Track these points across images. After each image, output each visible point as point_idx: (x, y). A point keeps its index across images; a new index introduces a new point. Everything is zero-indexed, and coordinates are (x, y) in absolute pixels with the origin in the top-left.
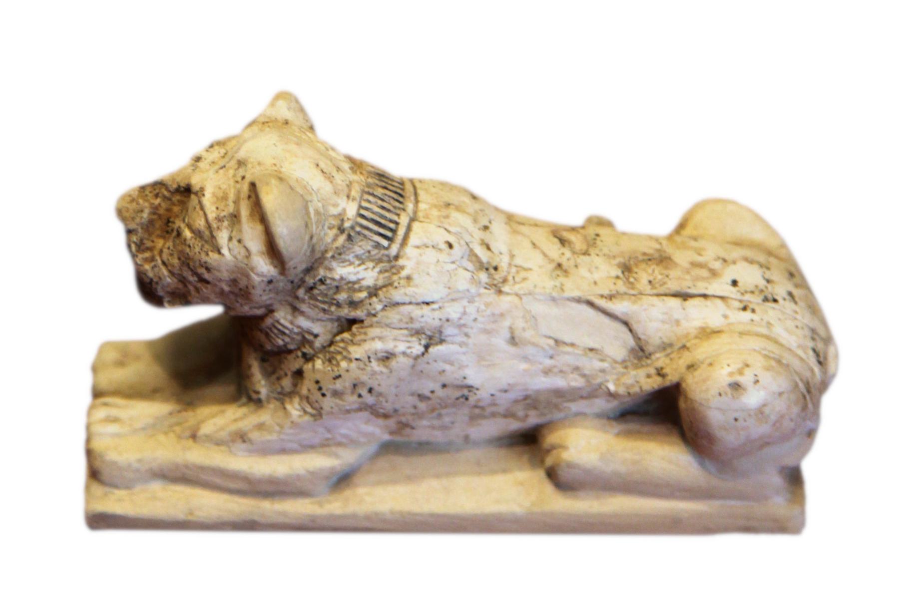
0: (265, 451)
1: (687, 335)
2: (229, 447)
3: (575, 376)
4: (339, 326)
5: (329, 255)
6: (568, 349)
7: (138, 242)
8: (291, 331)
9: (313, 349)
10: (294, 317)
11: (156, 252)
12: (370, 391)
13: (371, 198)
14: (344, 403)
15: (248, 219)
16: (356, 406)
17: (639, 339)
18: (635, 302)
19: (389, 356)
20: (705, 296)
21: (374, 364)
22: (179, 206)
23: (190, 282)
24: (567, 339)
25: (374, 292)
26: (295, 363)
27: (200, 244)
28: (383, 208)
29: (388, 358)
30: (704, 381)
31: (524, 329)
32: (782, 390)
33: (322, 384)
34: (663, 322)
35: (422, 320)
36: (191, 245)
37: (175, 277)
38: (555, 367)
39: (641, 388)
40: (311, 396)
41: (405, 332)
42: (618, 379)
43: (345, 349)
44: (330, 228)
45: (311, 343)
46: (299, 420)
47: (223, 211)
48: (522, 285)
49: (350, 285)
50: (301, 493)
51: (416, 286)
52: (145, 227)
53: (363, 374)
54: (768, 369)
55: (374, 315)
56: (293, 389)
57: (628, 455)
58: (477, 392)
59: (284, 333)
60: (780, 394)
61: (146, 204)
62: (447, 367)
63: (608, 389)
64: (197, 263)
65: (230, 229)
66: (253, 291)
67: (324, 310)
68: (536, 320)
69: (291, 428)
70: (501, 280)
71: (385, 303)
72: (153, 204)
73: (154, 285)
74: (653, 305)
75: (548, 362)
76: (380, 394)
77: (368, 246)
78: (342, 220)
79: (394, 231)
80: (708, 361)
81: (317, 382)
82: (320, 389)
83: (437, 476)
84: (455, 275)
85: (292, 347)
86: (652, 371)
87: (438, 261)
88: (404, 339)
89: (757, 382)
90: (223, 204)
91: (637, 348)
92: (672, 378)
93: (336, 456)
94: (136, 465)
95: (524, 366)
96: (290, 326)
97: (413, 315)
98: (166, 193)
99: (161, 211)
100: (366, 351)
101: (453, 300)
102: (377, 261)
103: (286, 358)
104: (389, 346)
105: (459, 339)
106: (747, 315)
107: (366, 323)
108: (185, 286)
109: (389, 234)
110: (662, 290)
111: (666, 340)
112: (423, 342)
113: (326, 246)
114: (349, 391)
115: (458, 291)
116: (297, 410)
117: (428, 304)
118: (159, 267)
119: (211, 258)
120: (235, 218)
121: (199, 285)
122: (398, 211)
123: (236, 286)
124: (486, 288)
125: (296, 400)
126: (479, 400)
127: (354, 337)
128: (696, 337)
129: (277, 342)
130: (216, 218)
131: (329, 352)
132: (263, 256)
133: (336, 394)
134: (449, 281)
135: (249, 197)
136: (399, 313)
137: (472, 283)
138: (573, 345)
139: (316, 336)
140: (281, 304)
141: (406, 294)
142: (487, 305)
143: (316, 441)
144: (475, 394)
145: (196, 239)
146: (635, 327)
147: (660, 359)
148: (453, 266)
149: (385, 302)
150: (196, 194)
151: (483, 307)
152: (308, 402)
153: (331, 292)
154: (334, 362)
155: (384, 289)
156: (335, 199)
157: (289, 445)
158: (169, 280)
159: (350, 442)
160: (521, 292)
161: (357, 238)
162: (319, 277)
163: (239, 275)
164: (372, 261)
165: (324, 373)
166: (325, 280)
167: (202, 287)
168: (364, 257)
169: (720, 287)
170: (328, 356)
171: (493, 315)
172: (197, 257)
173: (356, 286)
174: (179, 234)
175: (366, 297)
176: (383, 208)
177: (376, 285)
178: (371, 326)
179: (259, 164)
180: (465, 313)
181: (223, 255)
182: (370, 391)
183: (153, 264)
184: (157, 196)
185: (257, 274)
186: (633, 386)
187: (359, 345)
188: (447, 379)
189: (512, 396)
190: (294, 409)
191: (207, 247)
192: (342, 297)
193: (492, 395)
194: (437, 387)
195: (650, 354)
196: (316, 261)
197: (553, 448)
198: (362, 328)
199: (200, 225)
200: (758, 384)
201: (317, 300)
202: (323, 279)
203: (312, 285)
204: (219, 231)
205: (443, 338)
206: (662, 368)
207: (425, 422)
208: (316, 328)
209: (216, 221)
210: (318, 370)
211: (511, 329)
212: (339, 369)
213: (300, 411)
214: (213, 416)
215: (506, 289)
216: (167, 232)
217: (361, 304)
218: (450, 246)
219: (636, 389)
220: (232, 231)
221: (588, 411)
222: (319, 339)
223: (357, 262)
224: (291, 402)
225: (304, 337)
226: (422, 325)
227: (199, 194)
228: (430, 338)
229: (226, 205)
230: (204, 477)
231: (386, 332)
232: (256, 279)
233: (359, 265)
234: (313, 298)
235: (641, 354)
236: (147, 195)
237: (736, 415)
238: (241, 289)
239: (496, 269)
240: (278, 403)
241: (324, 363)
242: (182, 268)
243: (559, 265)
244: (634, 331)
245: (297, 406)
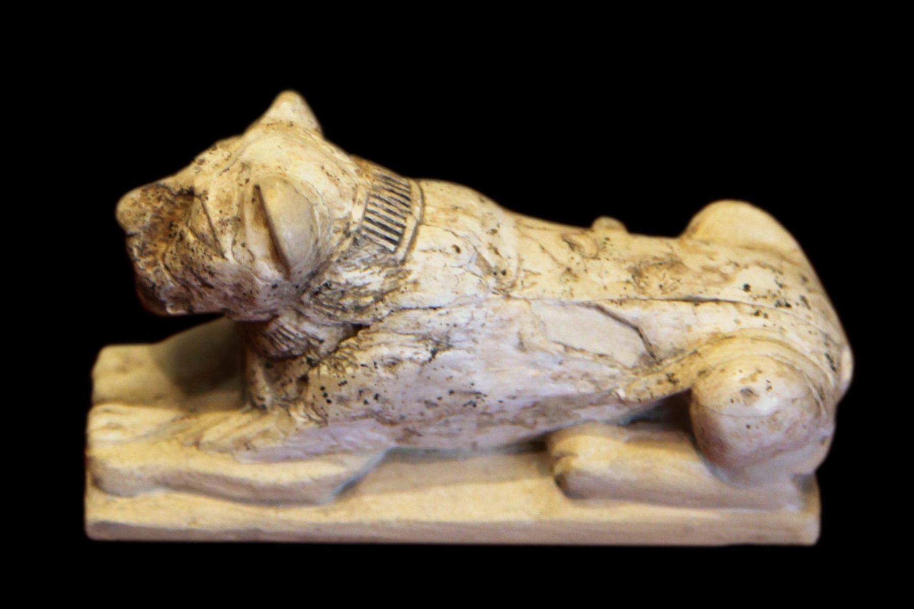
0: (269, 458)
1: (698, 341)
2: (233, 454)
3: (585, 382)
4: (344, 331)
5: (335, 259)
6: (578, 355)
7: (140, 246)
8: (296, 336)
9: (319, 355)
10: (299, 322)
11: (159, 257)
12: (377, 397)
13: (377, 201)
15: (252, 223)
16: (361, 413)
17: (650, 345)
18: (645, 307)
19: (396, 362)
20: (717, 301)
21: (380, 370)
22: (182, 209)
23: (193, 287)
24: (577, 345)
25: (380, 297)
26: (300, 369)
27: (203, 248)
28: (389, 211)
29: (394, 364)
30: (716, 387)
31: (533, 335)
32: (795, 397)
33: (327, 391)
34: (674, 327)
35: (430, 325)
36: (195, 249)
37: (178, 282)
38: (564, 373)
39: (651, 394)
40: (316, 403)
41: (412, 337)
42: (628, 386)
43: (351, 354)
44: (336, 232)
45: (316, 349)
46: (304, 427)
47: (227, 214)
48: (531, 290)
49: (356, 290)
50: (306, 501)
51: (423, 291)
52: (147, 231)
53: (369, 380)
54: (781, 375)
55: (381, 321)
56: (298, 396)
57: (638, 463)
58: (485, 399)
59: (289, 339)
60: (794, 401)
61: (149, 208)
62: (455, 373)
63: (619, 396)
64: (201, 268)
65: (234, 233)
66: (257, 296)
67: (330, 316)
68: (545, 325)
69: (296, 435)
70: (509, 285)
71: (392, 308)
72: (156, 207)
73: (157, 290)
74: (664, 311)
75: (557, 368)
76: (387, 401)
77: (374, 250)
78: (348, 224)
79: (400, 235)
80: (720, 367)
81: (323, 388)
82: (325, 395)
83: (445, 484)
84: (463, 279)
85: (296, 352)
86: (663, 377)
87: (445, 265)
88: (411, 344)
89: (769, 388)
90: (226, 207)
91: (648, 354)
92: (683, 384)
93: (342, 463)
94: (138, 473)
95: (532, 372)
96: (295, 332)
97: (420, 320)
98: (168, 196)
99: (164, 215)
100: (372, 357)
101: (461, 305)
102: (383, 265)
103: (291, 364)
104: (396, 351)
105: (467, 344)
106: (760, 320)
107: (372, 329)
108: (188, 291)
109: (396, 238)
110: (673, 295)
111: (677, 346)
112: (431, 348)
113: (331, 250)
114: (355, 398)
115: (466, 296)
116: (302, 416)
117: (435, 309)
118: (161, 271)
119: (214, 263)
120: (239, 221)
121: (202, 290)
122: (405, 215)
123: (240, 291)
124: (494, 293)
125: (301, 407)
126: (487, 407)
127: (360, 343)
128: (708, 343)
129: (282, 348)
130: (220, 222)
131: (335, 358)
132: (268, 261)
133: (342, 400)
134: (456, 286)
135: (253, 200)
136: (405, 318)
137: (480, 288)
138: (582, 351)
139: (321, 342)
140: (286, 309)
141: (412, 299)
142: (495, 310)
143: (322, 448)
144: (483, 400)
145: (199, 243)
146: (645, 332)
147: (671, 365)
148: (461, 271)
149: (392, 307)
150: (199, 197)
151: (491, 312)
152: (313, 409)
153: (336, 297)
155: (391, 294)
156: (341, 202)
157: (294, 453)
158: (171, 285)
159: (356, 450)
160: (530, 297)
161: (363, 242)
162: (325, 282)
163: (243, 280)
164: (379, 265)
165: (330, 379)
166: (331, 285)
167: (206, 292)
168: (370, 261)
169: (732, 292)
170: (333, 362)
171: (502, 320)
172: (200, 262)
173: (362, 291)
174: (182, 238)
175: (372, 302)
176: (389, 211)
177: (382, 290)
178: (377, 331)
179: (264, 166)
180: (472, 318)
181: (227, 259)
182: (377, 397)
183: (155, 268)
184: (159, 199)
185: (262, 279)
186: (643, 392)
187: (365, 350)
188: (455, 385)
189: (520, 402)
190: (299, 416)
191: (210, 251)
192: (348, 301)
193: (500, 402)
194: (444, 393)
195: (661, 360)
196: (321, 265)
197: (562, 455)
198: (368, 333)
199: (203, 229)
200: (771, 391)
201: (322, 305)
202: (329, 284)
203: (317, 289)
204: (223, 235)
205: (450, 343)
206: (673, 375)
207: (432, 430)
208: (322, 334)
209: (220, 225)
210: (324, 377)
211: (520, 335)
212: (345, 375)
213: (305, 418)
214: (217, 423)
215: (514, 293)
216: (170, 236)
217: (367, 310)
218: (458, 250)
219: (647, 396)
220: (236, 235)
221: (598, 417)
222: (324, 344)
223: (363, 267)
224: (296, 409)
225: (309, 343)
226: (429, 330)
227: (203, 197)
228: (438, 343)
229: (230, 209)
230: (207, 485)
231: (393, 338)
232: (260, 284)
233: (365, 270)
234: (319, 303)
235: (651, 360)
236: (149, 199)
237: (749, 422)
238: (245, 294)
239: (504, 273)
240: (282, 410)
241: (329, 369)
242: (185, 272)
243: (569, 270)
244: (645, 337)
245: (302, 413)
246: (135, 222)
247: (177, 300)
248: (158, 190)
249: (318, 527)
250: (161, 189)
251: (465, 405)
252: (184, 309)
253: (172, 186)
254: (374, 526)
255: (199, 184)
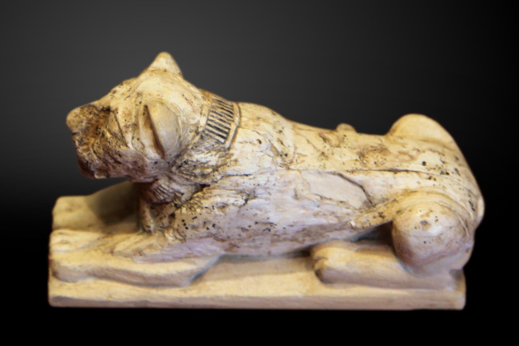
0: (153, 260)
1: (396, 194)
2: (132, 258)
3: (332, 217)
4: (195, 188)
5: (190, 147)
6: (328, 202)
7: (80, 140)
8: (168, 191)
9: (181, 202)
10: (170, 183)
11: (90, 146)
12: (214, 226)
13: (214, 114)
14: (199, 233)
15: (143, 127)
16: (205, 234)
17: (369, 196)
18: (366, 175)
19: (225, 205)
20: (407, 171)
21: (216, 210)
22: (104, 119)
23: (110, 163)
24: (327, 196)
25: (216, 169)
26: (170, 210)
27: (115, 141)
28: (221, 120)
29: (224, 207)
30: (407, 220)
31: (302, 190)
32: (451, 225)
33: (186, 222)
34: (383, 186)
35: (244, 185)
36: (111, 142)
37: (101, 160)
38: (320, 212)
39: (370, 224)
40: (179, 229)
41: (234, 192)
42: (357, 219)
43: (199, 201)
44: (191, 132)
45: (179, 198)
46: (173, 243)
47: (129, 122)
48: (302, 165)
49: (202, 165)
50: (174, 285)
51: (240, 165)
52: (84, 131)
53: (210, 216)
54: (443, 213)
55: (216, 182)
56: (169, 225)
57: (363, 263)
58: (276, 227)
59: (164, 193)
60: (451, 228)
61: (85, 118)
62: (258, 212)
63: (351, 225)
64: (114, 152)
65: (133, 133)
66: (146, 168)
67: (187, 179)
68: (309, 185)
69: (168, 247)
70: (289, 162)
71: (222, 175)
72: (89, 118)
73: (89, 165)
74: (377, 176)
75: (317, 209)
76: (220, 228)
77: (212, 142)
78: (198, 127)
79: (227, 134)
80: (409, 209)
81: (183, 221)
82: (185, 225)
83: (252, 275)
84: (263, 159)
85: (168, 200)
86: (377, 214)
87: (253, 151)
88: (233, 196)
89: (437, 220)
90: (129, 118)
91: (368, 201)
92: (388, 218)
93: (194, 263)
94: (78, 269)
95: (302, 211)
96: (167, 188)
97: (238, 182)
98: (96, 111)
99: (93, 122)
100: (211, 203)
101: (262, 173)
102: (217, 151)
103: (165, 207)
104: (225, 200)
105: (265, 196)
106: (432, 182)
107: (211, 187)
108: (107, 165)
109: (225, 135)
110: (382, 167)
111: (384, 197)
112: (244, 198)
113: (188, 142)
114: (201, 226)
115: (265, 168)
116: (171, 237)
117: (247, 175)
118: (92, 154)
119: (122, 149)
120: (136, 126)
121: (115, 165)
122: (230, 122)
123: (136, 165)
124: (280, 166)
125: (171, 231)
126: (276, 231)
127: (204, 195)
128: (402, 195)
129: (160, 198)
130: (125, 126)
131: (190, 203)
132: (152, 148)
133: (194, 227)
134: (259, 162)
135: (144, 114)
136: (230, 181)
137: (273, 164)
138: (331, 199)
139: (182, 194)
140: (162, 176)
141: (234, 170)
142: (281, 176)
143: (183, 254)
144: (274, 228)
145: (113, 138)
146: (367, 189)
147: (381, 208)
148: (262, 154)
149: (222, 174)
150: (113, 112)
151: (279, 177)
152: (178, 232)
153: (191, 169)
154: (193, 209)
155: (222, 167)
156: (193, 115)
157: (167, 257)
158: (97, 162)
159: (202, 256)
160: (301, 169)
161: (206, 138)
162: (184, 160)
163: (138, 159)
164: (215, 151)
165: (187, 215)
166: (188, 162)
167: (117, 166)
168: (210, 148)
169: (416, 166)
170: (189, 206)
171: (285, 182)
172: (113, 149)
173: (206, 165)
174: (103, 135)
175: (211, 172)
176: (221, 120)
177: (217, 165)
178: (214, 188)
179: (150, 95)
180: (268, 181)
181: (129, 147)
182: (214, 226)
183: (88, 152)
184: (90, 113)
185: (149, 159)
186: (365, 223)
187: (207, 199)
188: (258, 219)
189: (295, 228)
190: (170, 236)
191: (119, 143)
192: (197, 171)
193: (284, 228)
194: (252, 223)
195: (375, 205)
196: (183, 151)
197: (319, 259)
198: (209, 189)
199: (115, 130)
200: (438, 222)
201: (183, 173)
202: (187, 161)
203: (180, 164)
204: (126, 134)
205: (256, 195)
206: (382, 213)
207: (245, 244)
208: (183, 190)
209: (125, 128)
210: (184, 214)
211: (295, 190)
212: (196, 213)
213: (173, 237)
214: (123, 240)
215: (292, 167)
216: (97, 134)
217: (208, 176)
218: (260, 142)
219: (367, 225)
220: (134, 134)
221: (339, 237)
222: (184, 196)
223: (206, 152)
224: (168, 232)
225: (175, 195)
226: (244, 188)
227: (115, 112)
228: (248, 195)
229: (131, 119)
230: (118, 275)
231: (223, 192)
232: (148, 161)
233: (207, 153)
234: (181, 172)
235: (370, 204)
236: (85, 113)
237: (425, 240)
238: (139, 167)
239: (286, 155)
240: (160, 233)
241: (187, 210)
242: (105, 155)
243: (323, 153)
244: (366, 191)
245: (171, 234)
246: (77, 126)
247: (101, 170)
248: (90, 108)
249: (181, 299)
250: (92, 107)
251: (264, 230)
252: (105, 176)
253: (98, 106)
254: (212, 299)
255: (113, 105)
